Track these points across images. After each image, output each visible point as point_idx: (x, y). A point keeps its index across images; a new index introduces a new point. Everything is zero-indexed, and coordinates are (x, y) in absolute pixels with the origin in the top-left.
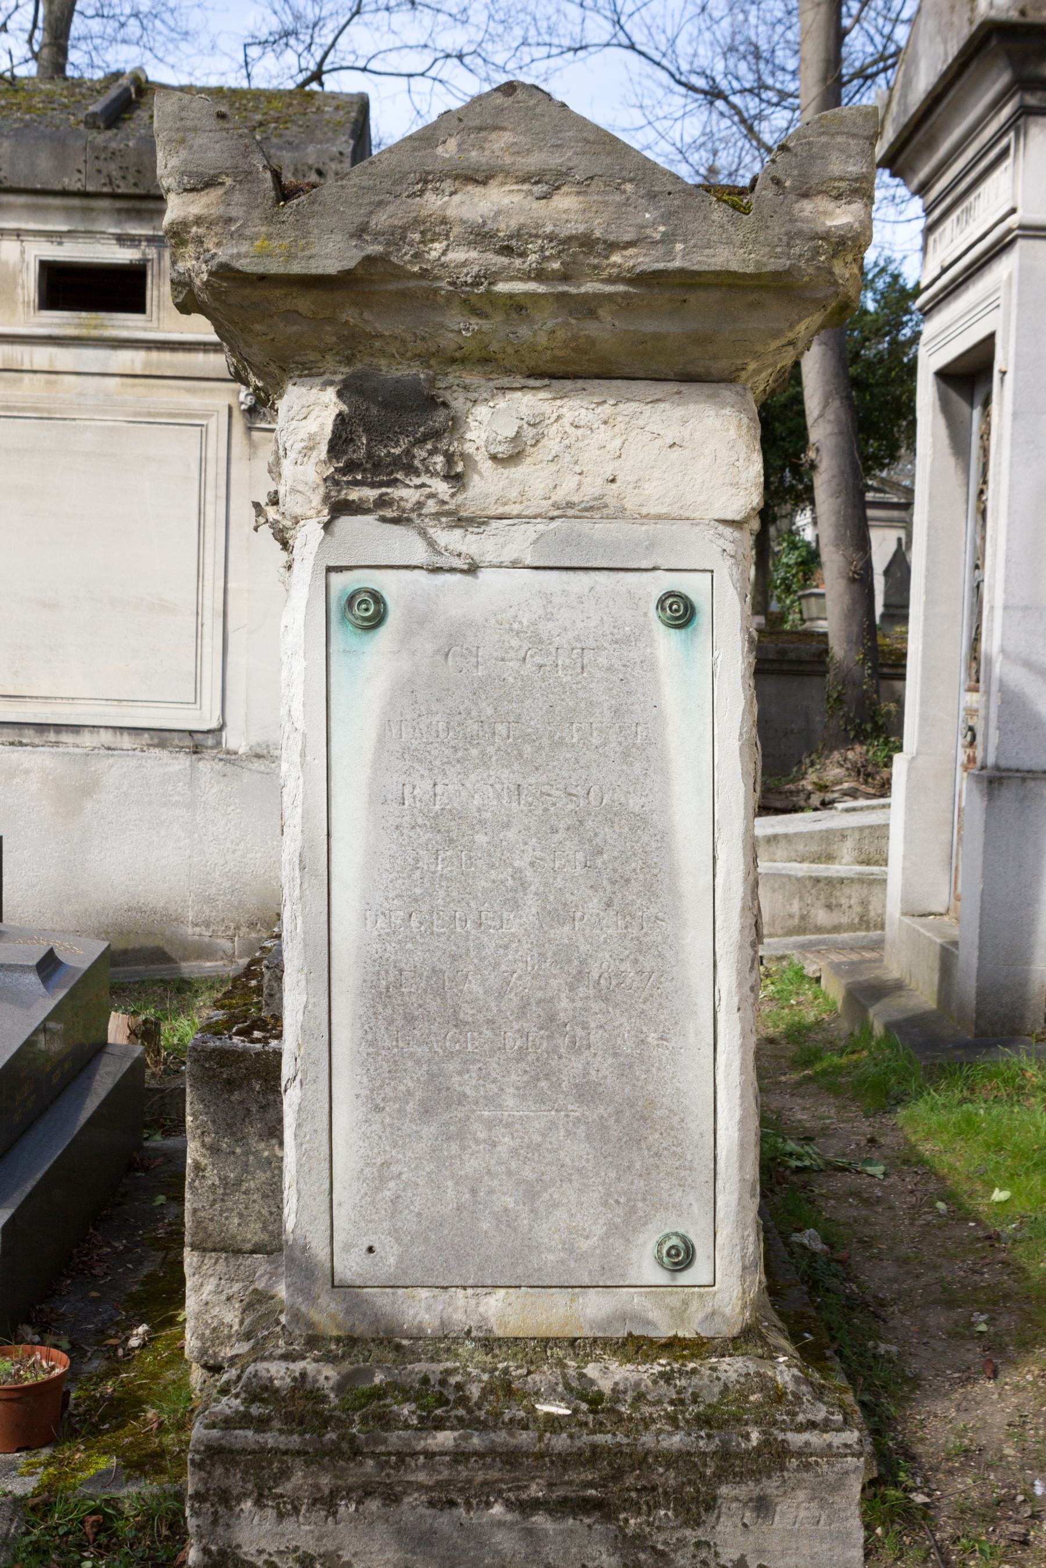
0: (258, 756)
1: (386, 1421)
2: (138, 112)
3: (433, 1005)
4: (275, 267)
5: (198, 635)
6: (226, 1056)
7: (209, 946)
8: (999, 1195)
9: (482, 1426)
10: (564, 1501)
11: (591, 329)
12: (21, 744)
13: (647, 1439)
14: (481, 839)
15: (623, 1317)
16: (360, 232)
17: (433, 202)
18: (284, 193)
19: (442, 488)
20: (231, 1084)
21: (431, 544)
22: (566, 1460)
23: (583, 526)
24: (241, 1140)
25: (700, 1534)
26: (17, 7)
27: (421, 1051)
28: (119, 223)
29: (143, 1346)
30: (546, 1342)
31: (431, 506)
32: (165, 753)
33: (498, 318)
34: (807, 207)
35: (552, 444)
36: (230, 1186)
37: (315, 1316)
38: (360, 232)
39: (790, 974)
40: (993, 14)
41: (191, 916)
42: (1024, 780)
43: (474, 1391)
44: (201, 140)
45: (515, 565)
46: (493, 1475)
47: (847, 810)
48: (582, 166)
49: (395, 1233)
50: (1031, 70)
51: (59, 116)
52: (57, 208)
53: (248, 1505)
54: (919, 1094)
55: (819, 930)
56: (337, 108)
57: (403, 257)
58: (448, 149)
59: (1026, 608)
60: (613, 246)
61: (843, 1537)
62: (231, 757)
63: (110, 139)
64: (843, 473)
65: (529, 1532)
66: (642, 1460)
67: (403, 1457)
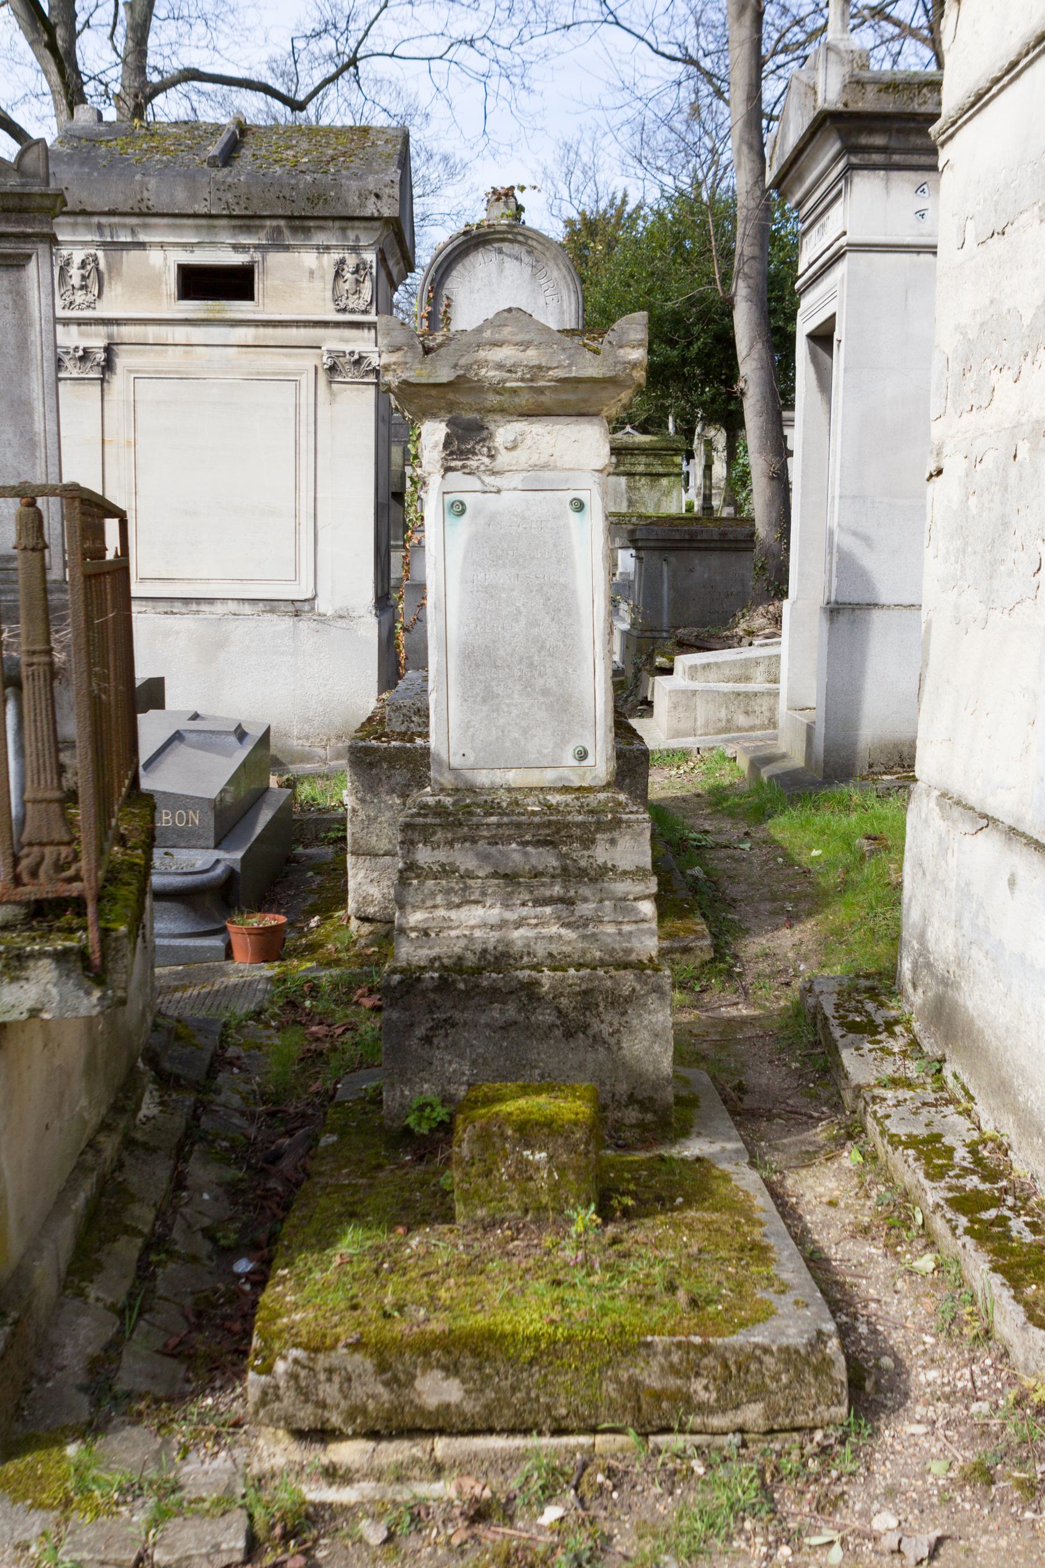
0: (341, 617)
1: (471, 814)
2: (243, 151)
3: (486, 660)
4: (424, 381)
5: (296, 532)
6: (368, 751)
7: (309, 753)
8: (815, 853)
9: (508, 815)
10: (538, 841)
11: (542, 398)
12: (172, 613)
13: (569, 818)
14: (504, 595)
15: (561, 779)
16: (455, 366)
17: (482, 354)
18: (427, 351)
19: (486, 460)
20: (371, 765)
21: (483, 482)
22: (539, 826)
23: (541, 473)
24: (377, 795)
25: (589, 853)
26: (97, 6)
27: (482, 678)
28: (234, 236)
29: (318, 927)
30: (531, 789)
31: (482, 468)
32: (275, 617)
33: (507, 395)
34: (621, 352)
35: (528, 442)
36: (371, 820)
37: (443, 781)
38: (455, 366)
39: (717, 757)
40: (826, 106)
41: (295, 732)
42: (853, 610)
43: (504, 804)
44: (396, 333)
45: (515, 489)
46: (512, 832)
47: (761, 645)
48: (537, 339)
49: (473, 748)
50: (853, 140)
51: (187, 157)
52: (190, 227)
53: (420, 845)
54: (782, 812)
55: (739, 729)
56: (387, 142)
57: (471, 375)
58: (487, 334)
59: (854, 497)
60: (549, 369)
61: (644, 853)
62: (322, 619)
63: (227, 176)
64: (764, 398)
65: (526, 854)
66: (568, 826)
67: (478, 826)
